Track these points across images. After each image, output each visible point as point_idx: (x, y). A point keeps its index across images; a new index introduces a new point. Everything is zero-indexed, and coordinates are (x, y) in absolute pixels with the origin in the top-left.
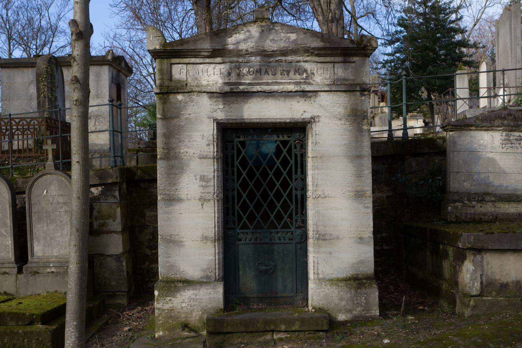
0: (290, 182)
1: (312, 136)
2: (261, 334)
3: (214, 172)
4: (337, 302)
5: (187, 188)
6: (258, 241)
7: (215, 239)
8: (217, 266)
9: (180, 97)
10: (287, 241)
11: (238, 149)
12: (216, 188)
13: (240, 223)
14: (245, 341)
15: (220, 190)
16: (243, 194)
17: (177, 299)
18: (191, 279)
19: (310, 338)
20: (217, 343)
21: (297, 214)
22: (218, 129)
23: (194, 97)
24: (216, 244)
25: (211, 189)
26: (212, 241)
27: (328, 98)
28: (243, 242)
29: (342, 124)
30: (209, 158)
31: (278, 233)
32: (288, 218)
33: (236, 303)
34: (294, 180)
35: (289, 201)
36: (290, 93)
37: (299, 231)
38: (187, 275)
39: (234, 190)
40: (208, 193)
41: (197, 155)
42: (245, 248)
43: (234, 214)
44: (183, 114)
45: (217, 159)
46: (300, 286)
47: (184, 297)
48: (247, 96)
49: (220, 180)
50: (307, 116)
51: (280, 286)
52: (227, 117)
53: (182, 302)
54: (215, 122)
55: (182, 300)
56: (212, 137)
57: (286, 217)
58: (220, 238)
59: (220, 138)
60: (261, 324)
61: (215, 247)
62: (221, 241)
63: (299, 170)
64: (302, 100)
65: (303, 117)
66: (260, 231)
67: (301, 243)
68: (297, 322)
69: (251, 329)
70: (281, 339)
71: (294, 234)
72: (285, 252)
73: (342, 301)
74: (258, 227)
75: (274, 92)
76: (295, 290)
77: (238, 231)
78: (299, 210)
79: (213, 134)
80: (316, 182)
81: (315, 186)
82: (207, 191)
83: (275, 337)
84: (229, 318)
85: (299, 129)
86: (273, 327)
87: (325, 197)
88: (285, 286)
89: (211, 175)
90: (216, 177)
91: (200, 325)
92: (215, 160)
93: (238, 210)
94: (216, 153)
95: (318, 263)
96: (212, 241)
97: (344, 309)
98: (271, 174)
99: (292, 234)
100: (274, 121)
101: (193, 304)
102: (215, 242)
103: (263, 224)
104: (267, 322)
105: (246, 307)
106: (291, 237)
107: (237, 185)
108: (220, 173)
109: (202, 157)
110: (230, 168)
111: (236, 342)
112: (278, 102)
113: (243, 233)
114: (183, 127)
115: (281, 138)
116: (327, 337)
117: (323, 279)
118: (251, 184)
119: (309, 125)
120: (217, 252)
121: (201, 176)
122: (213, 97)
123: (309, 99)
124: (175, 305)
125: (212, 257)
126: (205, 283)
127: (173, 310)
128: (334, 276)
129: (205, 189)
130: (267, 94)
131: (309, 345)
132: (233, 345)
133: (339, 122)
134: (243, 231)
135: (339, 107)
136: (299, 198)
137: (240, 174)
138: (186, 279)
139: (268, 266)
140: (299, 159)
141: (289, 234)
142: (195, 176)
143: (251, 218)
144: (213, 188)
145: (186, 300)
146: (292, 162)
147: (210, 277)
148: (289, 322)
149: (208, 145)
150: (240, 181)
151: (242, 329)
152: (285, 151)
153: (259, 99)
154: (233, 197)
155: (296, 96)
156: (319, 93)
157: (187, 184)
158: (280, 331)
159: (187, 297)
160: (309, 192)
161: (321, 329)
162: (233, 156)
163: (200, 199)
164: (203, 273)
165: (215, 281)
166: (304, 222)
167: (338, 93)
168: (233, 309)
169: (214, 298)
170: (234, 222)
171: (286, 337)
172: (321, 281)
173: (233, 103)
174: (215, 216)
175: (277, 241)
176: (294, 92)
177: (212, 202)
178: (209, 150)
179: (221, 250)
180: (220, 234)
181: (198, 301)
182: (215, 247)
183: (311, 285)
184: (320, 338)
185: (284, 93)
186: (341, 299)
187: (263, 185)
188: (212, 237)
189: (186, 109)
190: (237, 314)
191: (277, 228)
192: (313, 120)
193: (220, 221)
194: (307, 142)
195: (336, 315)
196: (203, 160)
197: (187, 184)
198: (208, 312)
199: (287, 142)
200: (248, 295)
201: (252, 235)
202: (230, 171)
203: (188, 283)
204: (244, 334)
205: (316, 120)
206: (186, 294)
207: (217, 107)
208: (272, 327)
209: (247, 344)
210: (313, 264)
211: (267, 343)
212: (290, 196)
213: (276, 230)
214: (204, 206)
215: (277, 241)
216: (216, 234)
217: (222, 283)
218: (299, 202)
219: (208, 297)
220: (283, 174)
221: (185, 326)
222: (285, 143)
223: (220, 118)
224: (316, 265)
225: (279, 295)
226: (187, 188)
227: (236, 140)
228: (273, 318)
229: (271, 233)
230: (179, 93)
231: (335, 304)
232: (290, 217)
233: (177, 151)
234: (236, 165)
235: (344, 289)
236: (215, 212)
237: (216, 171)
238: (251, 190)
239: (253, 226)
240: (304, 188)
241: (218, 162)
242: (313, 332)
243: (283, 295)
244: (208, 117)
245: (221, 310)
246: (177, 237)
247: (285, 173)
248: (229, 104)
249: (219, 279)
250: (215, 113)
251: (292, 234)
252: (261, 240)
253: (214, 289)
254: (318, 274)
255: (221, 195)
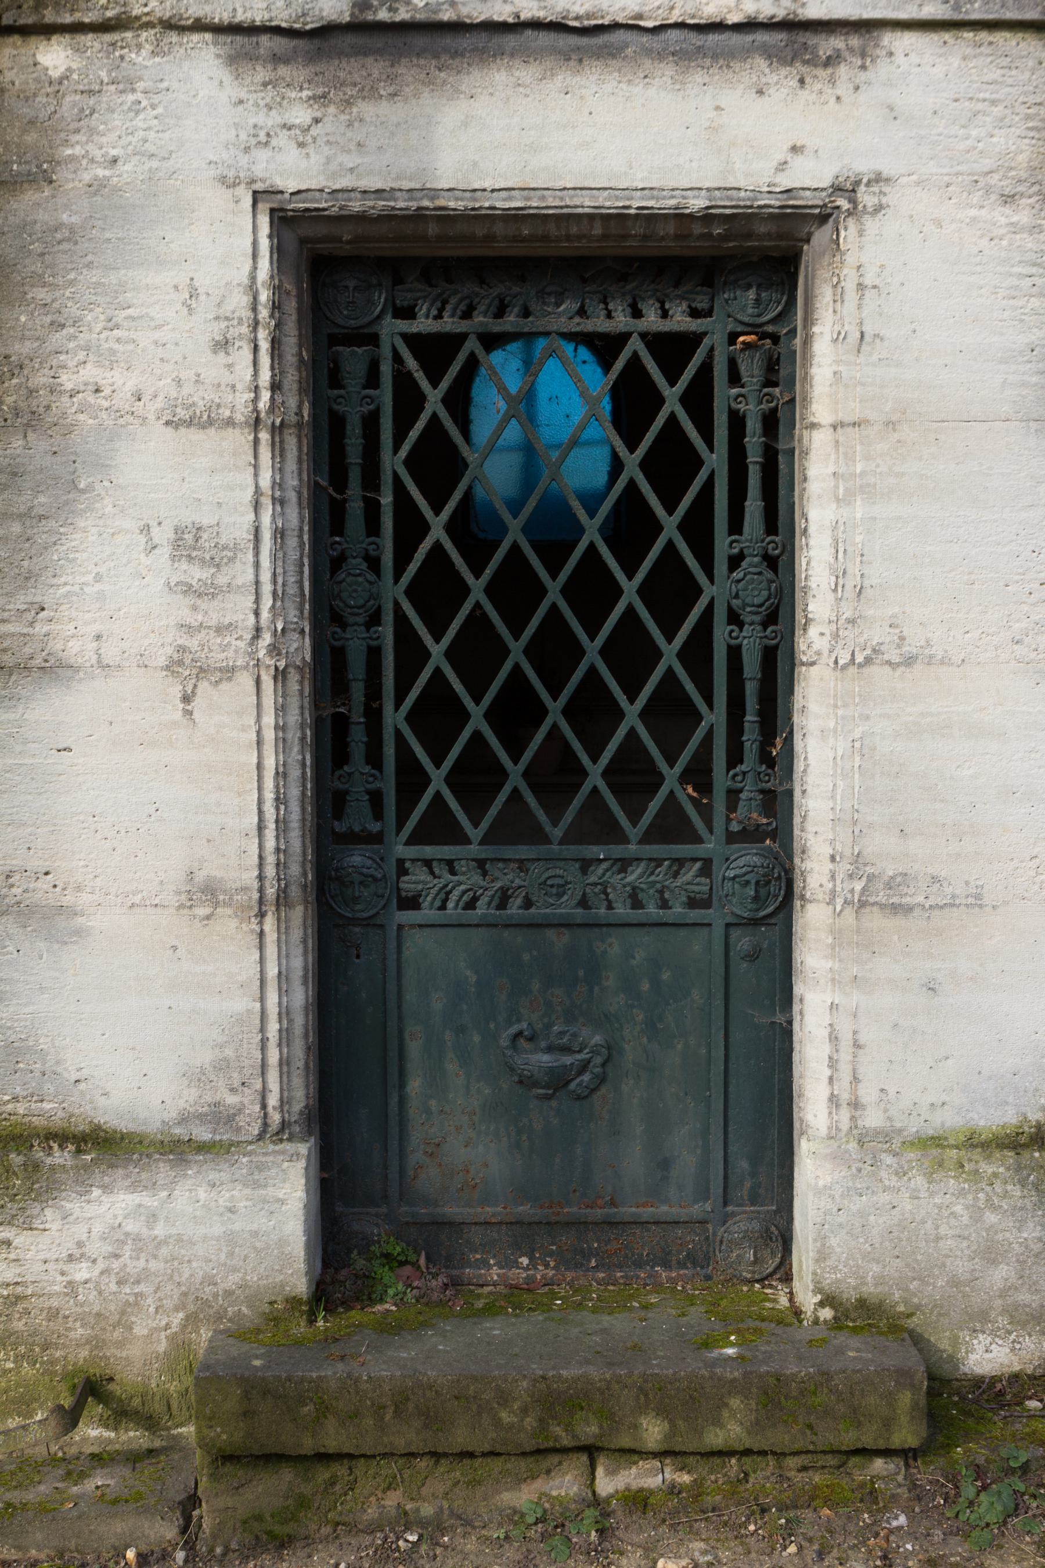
0: (702, 578)
1: (839, 297)
2: (523, 1464)
3: (257, 506)
4: (961, 1267)
5: (101, 597)
6: (514, 909)
7: (261, 901)
8: (273, 1056)
9: (54, 57)
10: (678, 909)
11: (404, 382)
12: (267, 602)
13: (696, 756)
14: (427, 1510)
15: (293, 614)
16: (427, 639)
17: (44, 1240)
18: (123, 1125)
19: (812, 1498)
20: (259, 1518)
21: (735, 757)
22: (279, 251)
23: (141, 55)
24: (270, 924)
25: (238, 610)
26: (243, 908)
27: (939, 71)
28: (427, 913)
29: (1015, 229)
30: (230, 422)
31: (624, 865)
32: (685, 777)
33: (387, 1256)
34: (721, 566)
35: (690, 687)
36: (713, 38)
37: (747, 859)
38: (102, 1101)
39: (375, 619)
40: (219, 630)
41: (159, 403)
42: (435, 953)
43: (375, 759)
44: (72, 158)
45: (277, 431)
46: (745, 1164)
47: (80, 1231)
48: (456, 54)
49: (293, 555)
50: (811, 176)
51: (634, 1160)
52: (334, 176)
53: (71, 1258)
54: (264, 207)
55: (69, 1246)
56: (245, 300)
57: (671, 775)
58: (295, 892)
59: (291, 306)
60: (525, 1411)
61: (261, 947)
62: (298, 914)
63: (753, 506)
64: (781, 81)
65: (785, 181)
66: (524, 851)
67: (755, 922)
68: (735, 1402)
69: (461, 1438)
70: (638, 1501)
71: (719, 871)
72: (666, 976)
73: (994, 1262)
74: (514, 828)
75: (615, 26)
76: (716, 1187)
77: (401, 850)
78: (751, 737)
79: (253, 278)
80: (854, 569)
81: (850, 593)
82: (214, 619)
83: (606, 1484)
84: (332, 1372)
85: (755, 260)
86: (594, 1429)
87: (909, 661)
88: (665, 1164)
89: (238, 524)
90: (267, 536)
91: (173, 1387)
92: (264, 436)
93: (398, 733)
94: (266, 396)
95: (857, 1045)
96: (243, 908)
97: (1005, 1311)
98: (592, 648)
99: (706, 870)
100: (609, 203)
101: (135, 1267)
102: (261, 915)
103: (541, 816)
104: (556, 1401)
105: (442, 1279)
106: (702, 886)
107: (393, 592)
108: (293, 515)
109: (192, 420)
110: (354, 489)
111: (372, 1512)
112: (637, 90)
113: (428, 863)
114: (73, 235)
115: (651, 320)
116: (917, 1493)
117: (885, 1136)
118: (477, 586)
119: (821, 236)
120: (272, 971)
121: (179, 531)
122: (251, 58)
123: (820, 72)
124: (33, 1271)
125: (245, 1004)
126: (203, 1148)
127: (19, 1298)
128: (949, 1119)
129: (203, 604)
130: (573, 40)
131: (810, 1554)
132: (353, 1528)
133: (1002, 216)
134: (429, 851)
135: (1000, 123)
136: (751, 666)
137: (410, 528)
138: (98, 1128)
139: (566, 1050)
140: (753, 440)
141: (690, 873)
142: (146, 529)
143: (476, 778)
144: (250, 598)
145: (96, 1248)
146: (716, 460)
147: (231, 1119)
148: (688, 1401)
149: (223, 345)
150: (413, 568)
151: (407, 1436)
152: (672, 395)
153: (527, 73)
154: (374, 654)
155: (745, 54)
156: (888, 39)
157: (98, 578)
158: (633, 1454)
159: (98, 1229)
160: (813, 632)
161: (881, 1445)
162: (371, 422)
163: (172, 667)
164: (191, 1095)
165: (260, 1137)
166: (778, 804)
167: (1000, 37)
168: (365, 1293)
169: (255, 1234)
170: (376, 799)
171: (673, 1490)
172: (866, 1145)
173: (371, 93)
174: (260, 766)
175: (622, 911)
176: (738, 27)
177: (246, 681)
178: (227, 378)
179: (297, 963)
180: (295, 869)
181: (164, 1251)
182: (261, 947)
183: (814, 1172)
184: (870, 1496)
185: (674, 34)
186: (991, 1253)
187: (542, 591)
188: (244, 889)
189: (92, 131)
190: (388, 1328)
191: (623, 839)
192: (844, 203)
193: (295, 792)
194: (807, 341)
195: (955, 1341)
196: (194, 435)
197: (98, 578)
198: (219, 1317)
199: (689, 342)
200: (452, 1210)
201: (477, 879)
202: (355, 507)
203: (103, 1146)
204: (422, 1464)
205: (866, 198)
206: (91, 1210)
207: (274, 118)
208: (589, 1430)
209: (433, 1530)
210: (826, 1049)
211: (553, 1523)
212: (697, 653)
213: (618, 851)
214: (198, 704)
215: (622, 911)
216: (270, 871)
217: (303, 1148)
218: (751, 689)
219: (217, 1230)
220: (658, 528)
221: (92, 1390)
222: (672, 350)
223: (292, 186)
224: (845, 1056)
225: (627, 1211)
226: (101, 597)
227: (392, 330)
228: (595, 1372)
229: (586, 865)
230: (48, 30)
231: (954, 1282)
232: (699, 775)
233: (41, 379)
234: (387, 478)
235: (1006, 1195)
236: (259, 743)
237: (267, 502)
238: (477, 619)
239: (485, 824)
240: (780, 612)
241: (278, 450)
242: (831, 1461)
243: (647, 1212)
244: (222, 179)
245: (293, 1302)
246: (45, 883)
247: (670, 524)
248: (348, 103)
249: (284, 1125)
250: (262, 155)
251: (706, 870)
252: (528, 904)
253: (257, 1185)
254: (855, 1105)
255: (300, 647)
